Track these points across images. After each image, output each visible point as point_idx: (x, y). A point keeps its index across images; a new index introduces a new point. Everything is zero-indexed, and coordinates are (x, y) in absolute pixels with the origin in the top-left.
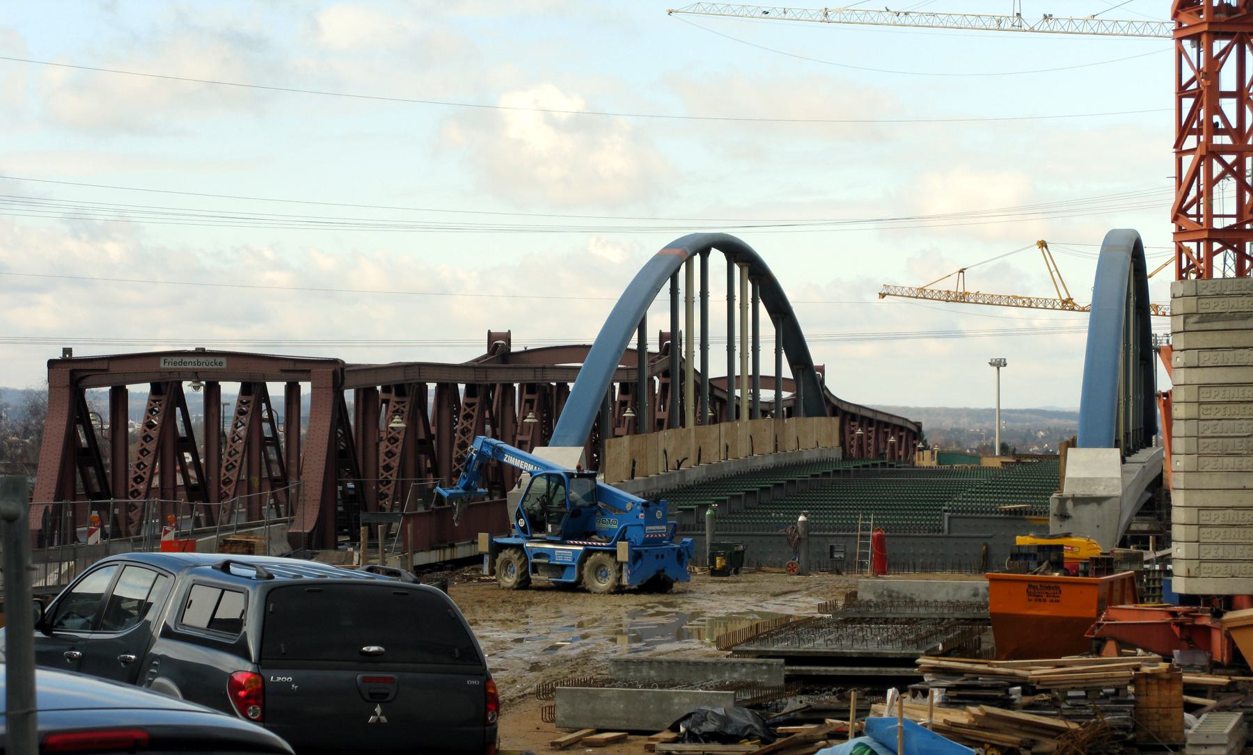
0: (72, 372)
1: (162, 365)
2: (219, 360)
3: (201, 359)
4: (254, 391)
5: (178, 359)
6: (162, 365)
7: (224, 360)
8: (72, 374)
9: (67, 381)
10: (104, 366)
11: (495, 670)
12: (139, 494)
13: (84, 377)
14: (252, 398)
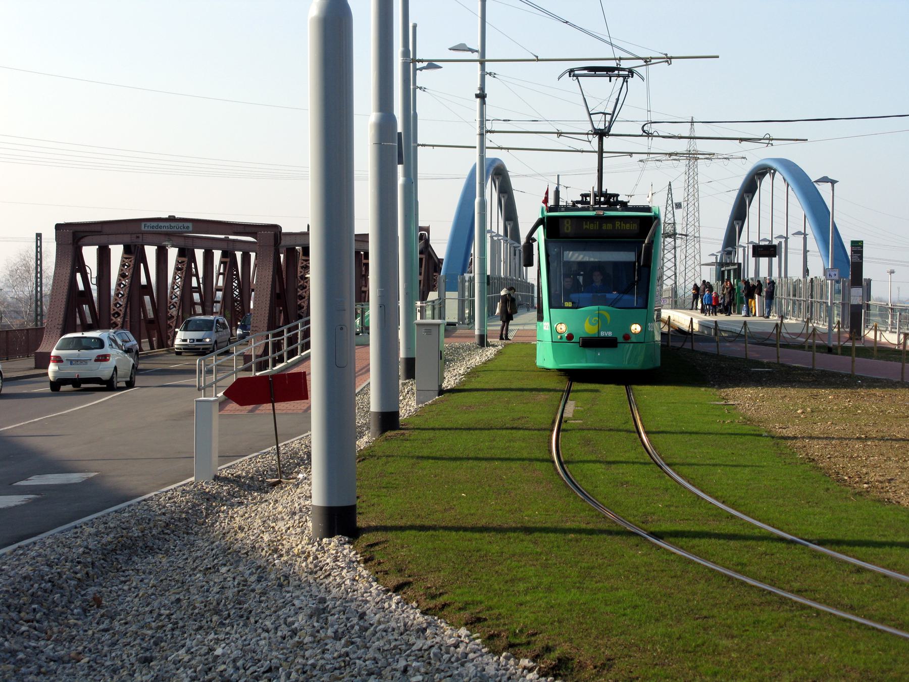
0: (74, 234)
1: (143, 228)
2: (186, 224)
3: (173, 224)
4: (135, 254)
5: (155, 224)
6: (143, 228)
7: (190, 225)
8: (72, 236)
9: (70, 241)
10: (98, 228)
11: (806, 271)
12: (117, 325)
13: (83, 237)
14: (185, 259)
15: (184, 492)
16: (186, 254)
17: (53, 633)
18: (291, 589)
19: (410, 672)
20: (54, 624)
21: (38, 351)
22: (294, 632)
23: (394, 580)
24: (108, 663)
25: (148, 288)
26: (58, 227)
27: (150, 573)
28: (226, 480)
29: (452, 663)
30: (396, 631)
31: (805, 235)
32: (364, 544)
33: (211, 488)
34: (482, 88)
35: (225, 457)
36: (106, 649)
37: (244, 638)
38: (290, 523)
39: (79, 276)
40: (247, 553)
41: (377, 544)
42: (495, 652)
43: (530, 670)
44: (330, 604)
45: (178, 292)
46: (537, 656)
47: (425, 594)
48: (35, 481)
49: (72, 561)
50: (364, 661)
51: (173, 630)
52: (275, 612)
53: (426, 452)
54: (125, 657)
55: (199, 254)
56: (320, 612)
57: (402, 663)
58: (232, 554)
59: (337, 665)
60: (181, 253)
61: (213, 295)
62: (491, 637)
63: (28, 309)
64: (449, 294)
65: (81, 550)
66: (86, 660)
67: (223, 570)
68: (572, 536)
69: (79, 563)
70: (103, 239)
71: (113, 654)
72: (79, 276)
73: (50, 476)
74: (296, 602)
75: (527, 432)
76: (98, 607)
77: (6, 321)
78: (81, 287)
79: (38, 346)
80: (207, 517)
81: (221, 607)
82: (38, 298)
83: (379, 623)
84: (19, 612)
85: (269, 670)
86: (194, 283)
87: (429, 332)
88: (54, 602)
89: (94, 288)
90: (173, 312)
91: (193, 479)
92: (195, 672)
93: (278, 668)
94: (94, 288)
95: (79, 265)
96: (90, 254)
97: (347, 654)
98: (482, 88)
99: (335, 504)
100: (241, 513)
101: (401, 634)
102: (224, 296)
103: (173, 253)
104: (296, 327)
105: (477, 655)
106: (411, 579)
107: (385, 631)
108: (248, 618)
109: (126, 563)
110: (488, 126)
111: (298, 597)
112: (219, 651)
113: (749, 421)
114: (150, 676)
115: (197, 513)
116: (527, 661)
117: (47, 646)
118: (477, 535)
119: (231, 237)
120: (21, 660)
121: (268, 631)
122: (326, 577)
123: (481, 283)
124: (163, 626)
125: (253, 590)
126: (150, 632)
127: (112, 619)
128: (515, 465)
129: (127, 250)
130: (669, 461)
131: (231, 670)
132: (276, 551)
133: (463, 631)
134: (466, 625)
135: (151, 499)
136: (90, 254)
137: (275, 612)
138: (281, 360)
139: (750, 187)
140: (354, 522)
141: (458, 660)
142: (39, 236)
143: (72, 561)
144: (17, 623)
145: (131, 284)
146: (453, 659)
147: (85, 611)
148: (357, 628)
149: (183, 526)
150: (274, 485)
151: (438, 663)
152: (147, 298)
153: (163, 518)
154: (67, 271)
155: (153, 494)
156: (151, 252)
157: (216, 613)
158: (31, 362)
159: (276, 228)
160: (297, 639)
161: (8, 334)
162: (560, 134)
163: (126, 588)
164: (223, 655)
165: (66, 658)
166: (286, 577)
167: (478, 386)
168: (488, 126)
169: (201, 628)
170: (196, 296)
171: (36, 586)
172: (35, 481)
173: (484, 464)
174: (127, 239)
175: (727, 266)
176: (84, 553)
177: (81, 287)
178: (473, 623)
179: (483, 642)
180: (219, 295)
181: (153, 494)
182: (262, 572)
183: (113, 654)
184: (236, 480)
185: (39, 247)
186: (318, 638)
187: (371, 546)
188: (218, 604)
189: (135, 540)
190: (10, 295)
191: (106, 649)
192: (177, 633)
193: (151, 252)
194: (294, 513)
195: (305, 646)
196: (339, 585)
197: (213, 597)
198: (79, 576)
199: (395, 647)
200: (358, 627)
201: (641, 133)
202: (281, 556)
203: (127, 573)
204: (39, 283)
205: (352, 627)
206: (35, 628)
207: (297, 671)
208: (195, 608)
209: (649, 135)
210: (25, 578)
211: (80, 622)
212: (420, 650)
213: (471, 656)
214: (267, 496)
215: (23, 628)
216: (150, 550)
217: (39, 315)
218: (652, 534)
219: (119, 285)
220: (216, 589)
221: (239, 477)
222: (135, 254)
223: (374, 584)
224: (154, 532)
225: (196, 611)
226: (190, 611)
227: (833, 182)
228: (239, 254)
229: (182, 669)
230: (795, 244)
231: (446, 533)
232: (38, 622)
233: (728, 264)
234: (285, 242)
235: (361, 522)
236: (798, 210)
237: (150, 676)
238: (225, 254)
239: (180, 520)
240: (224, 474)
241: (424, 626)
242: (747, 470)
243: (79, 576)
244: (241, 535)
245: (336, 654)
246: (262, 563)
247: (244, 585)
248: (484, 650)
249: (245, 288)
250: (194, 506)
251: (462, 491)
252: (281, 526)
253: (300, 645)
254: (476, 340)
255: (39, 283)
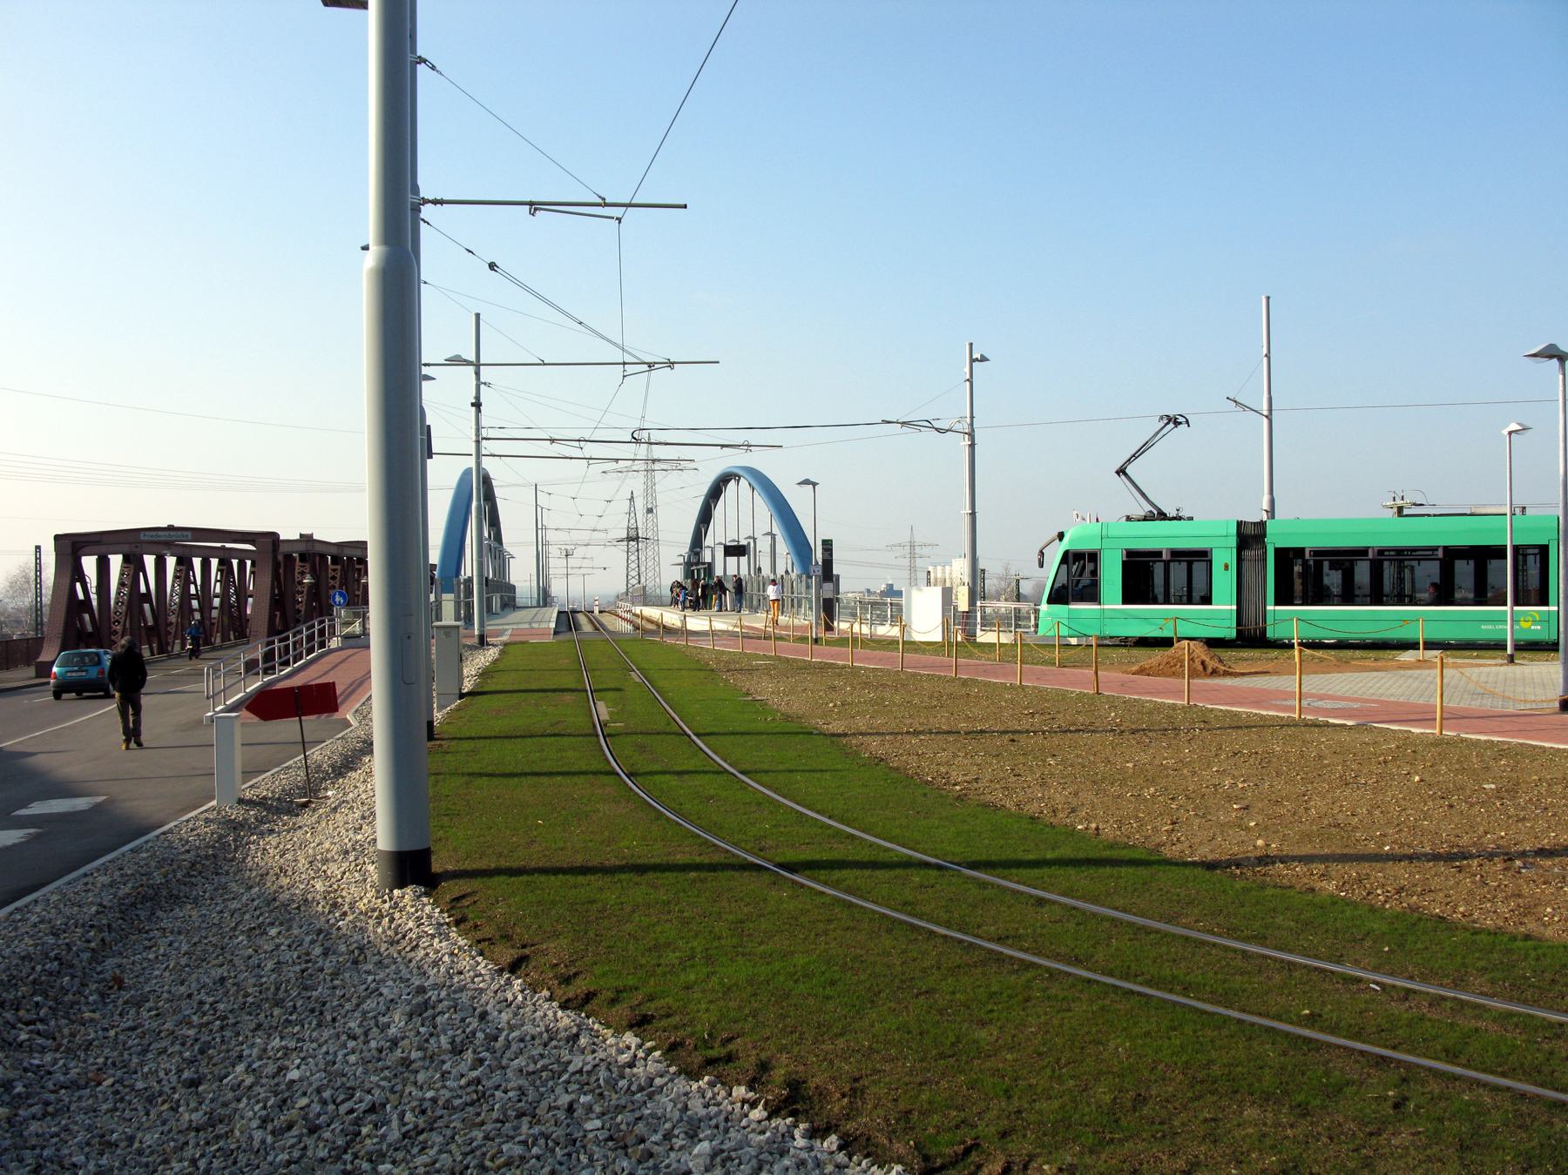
0: (74, 544)
4: (134, 564)
8: (71, 547)
15: (207, 820)
16: (184, 563)
17: (63, 1037)
18: (370, 967)
19: (579, 1112)
20: (64, 1022)
21: (41, 659)
22: (395, 1043)
23: (508, 954)
24: (140, 1085)
25: (147, 597)
26: (57, 538)
27: (180, 933)
28: (250, 803)
29: (634, 1093)
30: (537, 1041)
31: (773, 537)
32: (448, 898)
33: (237, 813)
34: (478, 397)
35: (248, 774)
36: (135, 1060)
37: (324, 1049)
38: (345, 865)
39: (78, 585)
40: (298, 908)
41: (463, 897)
42: (694, 1076)
43: (753, 1105)
44: (433, 995)
45: (176, 599)
46: (754, 1080)
47: (556, 977)
48: (37, 808)
49: (83, 926)
50: (505, 1092)
51: (222, 1028)
52: (358, 1005)
53: (475, 768)
54: (162, 1074)
55: (197, 562)
56: (422, 1009)
57: (565, 1099)
58: (285, 911)
59: (468, 1099)
60: (179, 562)
61: (211, 602)
62: (673, 1047)
63: (28, 619)
64: (445, 596)
65: (94, 909)
66: (110, 1081)
67: (273, 932)
68: (693, 875)
69: (92, 926)
70: (103, 549)
71: (146, 1069)
72: (78, 585)
73: (54, 802)
74: (385, 991)
75: (572, 739)
76: (120, 989)
77: (6, 630)
78: (81, 596)
79: (38, 655)
80: (236, 850)
81: (281, 995)
82: (38, 608)
83: (512, 1028)
84: (17, 1010)
85: (372, 1109)
86: (193, 591)
87: (447, 635)
88: (62, 988)
89: (94, 597)
90: (173, 619)
91: (214, 803)
92: (265, 1107)
93: (384, 1105)
94: (94, 597)
95: (79, 575)
96: (89, 564)
97: (478, 1081)
98: (478, 397)
99: (406, 848)
100: (274, 843)
101: (545, 1045)
102: (222, 603)
103: (171, 562)
104: (301, 632)
105: (665, 1080)
106: (527, 951)
107: (522, 1040)
108: (321, 1013)
109: (149, 919)
110: (484, 433)
111: (383, 981)
112: (294, 1074)
113: (787, 718)
114: (201, 1113)
115: (225, 847)
116: (743, 1089)
117: (55, 1061)
118: (581, 879)
119: (228, 545)
120: (19, 1094)
121: (355, 1038)
122: (413, 949)
123: (480, 584)
124: (208, 1023)
125: (322, 970)
126: (191, 1032)
127: (139, 1005)
128: (580, 780)
129: (126, 560)
130: (747, 767)
131: (316, 1108)
132: (335, 905)
133: (630, 1038)
134: (631, 1027)
135: (170, 831)
136: (89, 564)
137: (358, 1005)
138: (286, 663)
139: (715, 493)
140: (429, 864)
141: (641, 1089)
142: (38, 548)
143: (83, 926)
144: (14, 1027)
145: (130, 593)
146: (634, 1088)
147: (102, 995)
148: (480, 1035)
149: (215, 862)
150: (305, 805)
151: (614, 1096)
152: (147, 606)
153: (187, 856)
154: (67, 581)
155: (172, 825)
156: (149, 561)
157: (277, 1005)
158: (31, 671)
159: (274, 535)
160: (398, 1053)
161: (8, 643)
162: (552, 441)
163: (151, 956)
164: (301, 1080)
165: (82, 1082)
166: (361, 949)
167: (499, 688)
168: (484, 433)
169: (259, 1026)
170: (195, 603)
171: (39, 968)
172: (37, 808)
173: (544, 780)
174: (126, 548)
175: (695, 563)
176: (98, 912)
177: (81, 596)
178: (640, 1024)
179: (663, 1054)
180: (216, 602)
181: (172, 825)
182: (324, 934)
183: (146, 1069)
184: (261, 803)
185: (38, 559)
186: (429, 1053)
187: (458, 899)
188: (278, 989)
189: (157, 889)
190: (11, 605)
191: (135, 1060)
192: (228, 1034)
193: (149, 561)
194: (347, 852)
195: (414, 1066)
196: (436, 964)
197: (269, 979)
198: (93, 945)
199: (545, 1068)
200: (481, 1038)
201: (629, 438)
202: (345, 914)
203: (151, 934)
204: (39, 594)
205: (474, 1033)
206: (38, 1033)
207: (413, 1110)
208: (246, 995)
209: (637, 441)
210: (23, 958)
211: (97, 1016)
212: (580, 1071)
213: (658, 1081)
214: (300, 820)
215: (23, 1036)
216: (176, 900)
217: (39, 625)
218: (781, 866)
219: (118, 593)
220: (270, 965)
221: (265, 798)
222: (134, 564)
223: (480, 959)
224: (179, 875)
225: (250, 999)
226: (241, 1000)
227: (814, 484)
228: (235, 562)
229: (245, 1100)
230: (764, 545)
231: (543, 878)
232: (42, 1021)
233: (698, 563)
234: (283, 549)
235: (436, 867)
236: (764, 510)
237: (201, 1113)
238: (221, 563)
239: (207, 857)
240: (248, 795)
241: (575, 1030)
242: (827, 775)
243: (93, 945)
244: (285, 881)
245: (463, 1082)
246: (320, 924)
247: (307, 962)
248: (673, 1069)
249: (242, 593)
250: (221, 837)
251: (537, 817)
252: (334, 869)
253: (406, 1063)
254: (476, 640)
255: (39, 594)
